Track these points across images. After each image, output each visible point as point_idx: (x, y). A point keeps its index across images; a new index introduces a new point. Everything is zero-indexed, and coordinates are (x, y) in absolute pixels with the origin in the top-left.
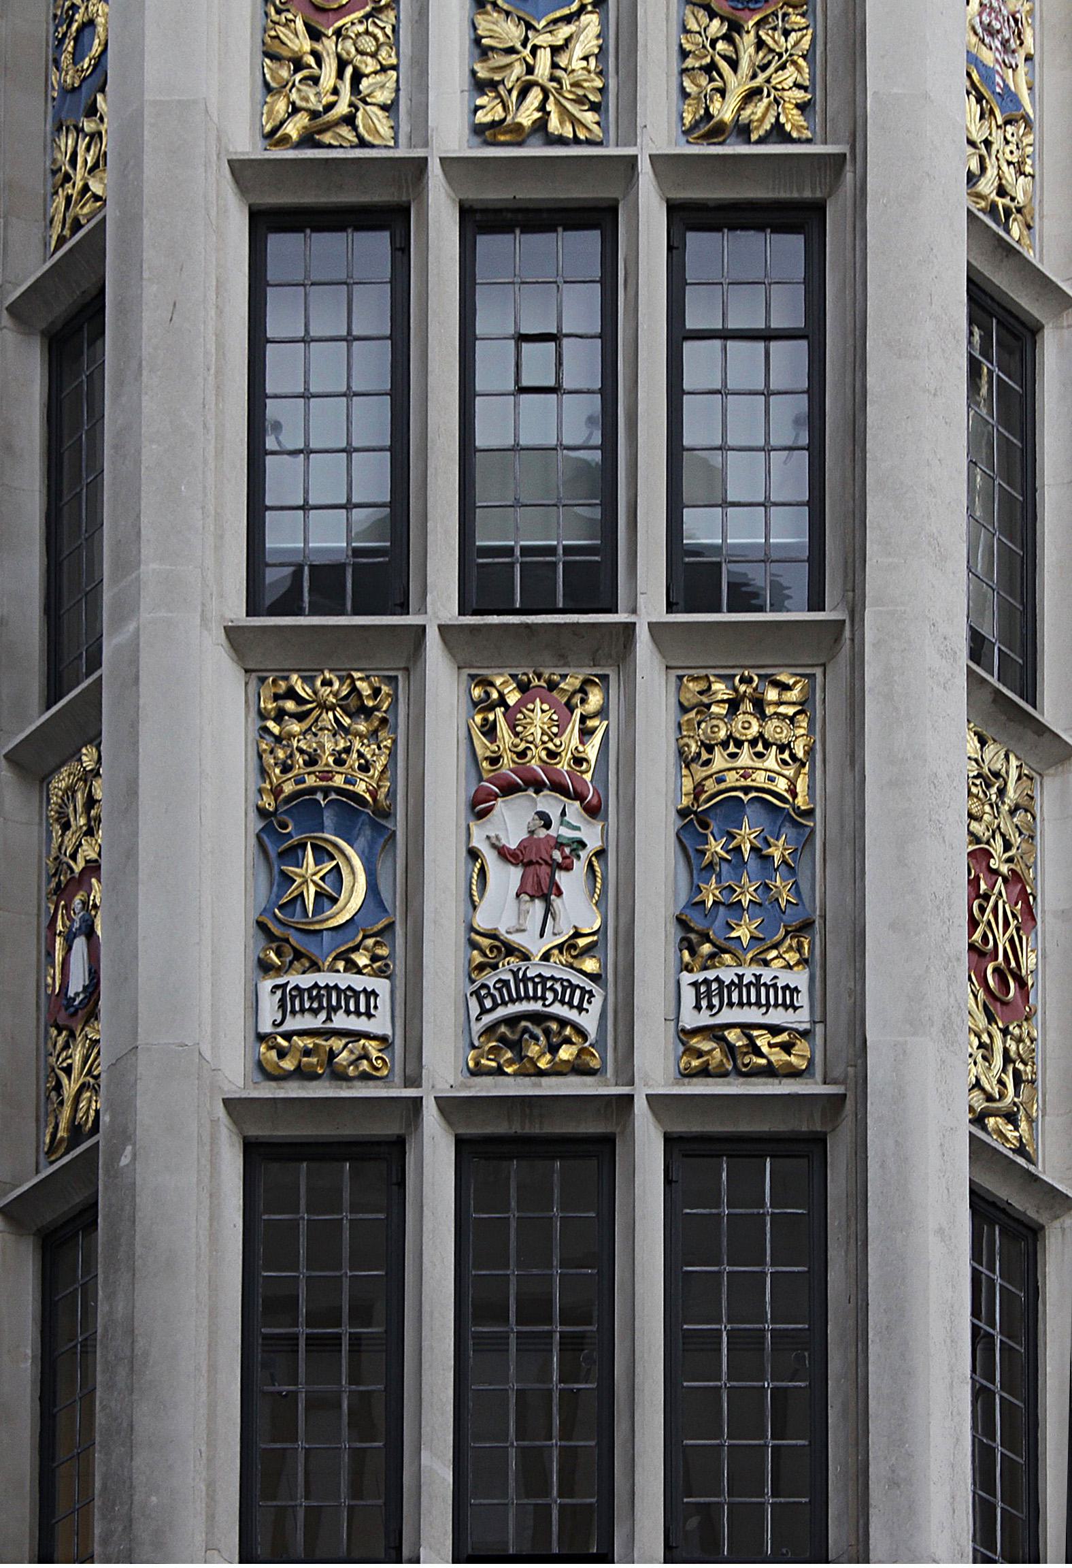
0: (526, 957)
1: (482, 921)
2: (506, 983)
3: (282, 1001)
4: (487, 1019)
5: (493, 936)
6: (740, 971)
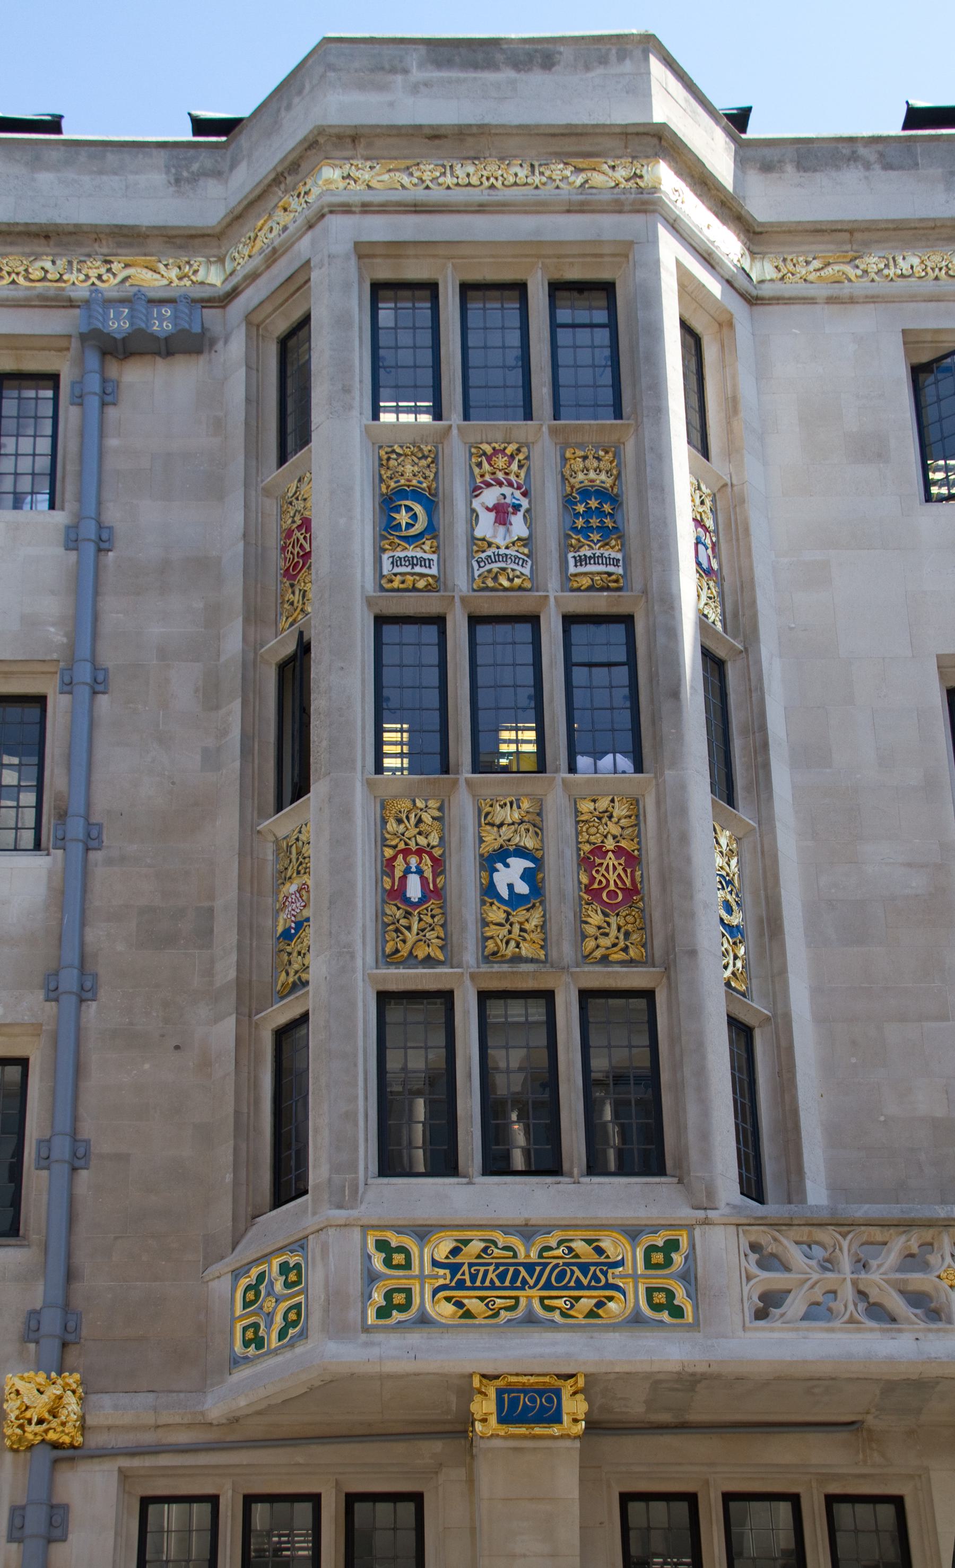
0: (498, 548)
1: (478, 533)
2: (490, 557)
3: (392, 563)
4: (482, 570)
5: (483, 539)
6: (594, 552)
